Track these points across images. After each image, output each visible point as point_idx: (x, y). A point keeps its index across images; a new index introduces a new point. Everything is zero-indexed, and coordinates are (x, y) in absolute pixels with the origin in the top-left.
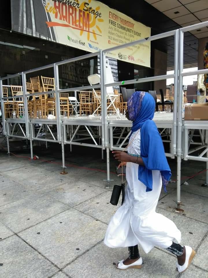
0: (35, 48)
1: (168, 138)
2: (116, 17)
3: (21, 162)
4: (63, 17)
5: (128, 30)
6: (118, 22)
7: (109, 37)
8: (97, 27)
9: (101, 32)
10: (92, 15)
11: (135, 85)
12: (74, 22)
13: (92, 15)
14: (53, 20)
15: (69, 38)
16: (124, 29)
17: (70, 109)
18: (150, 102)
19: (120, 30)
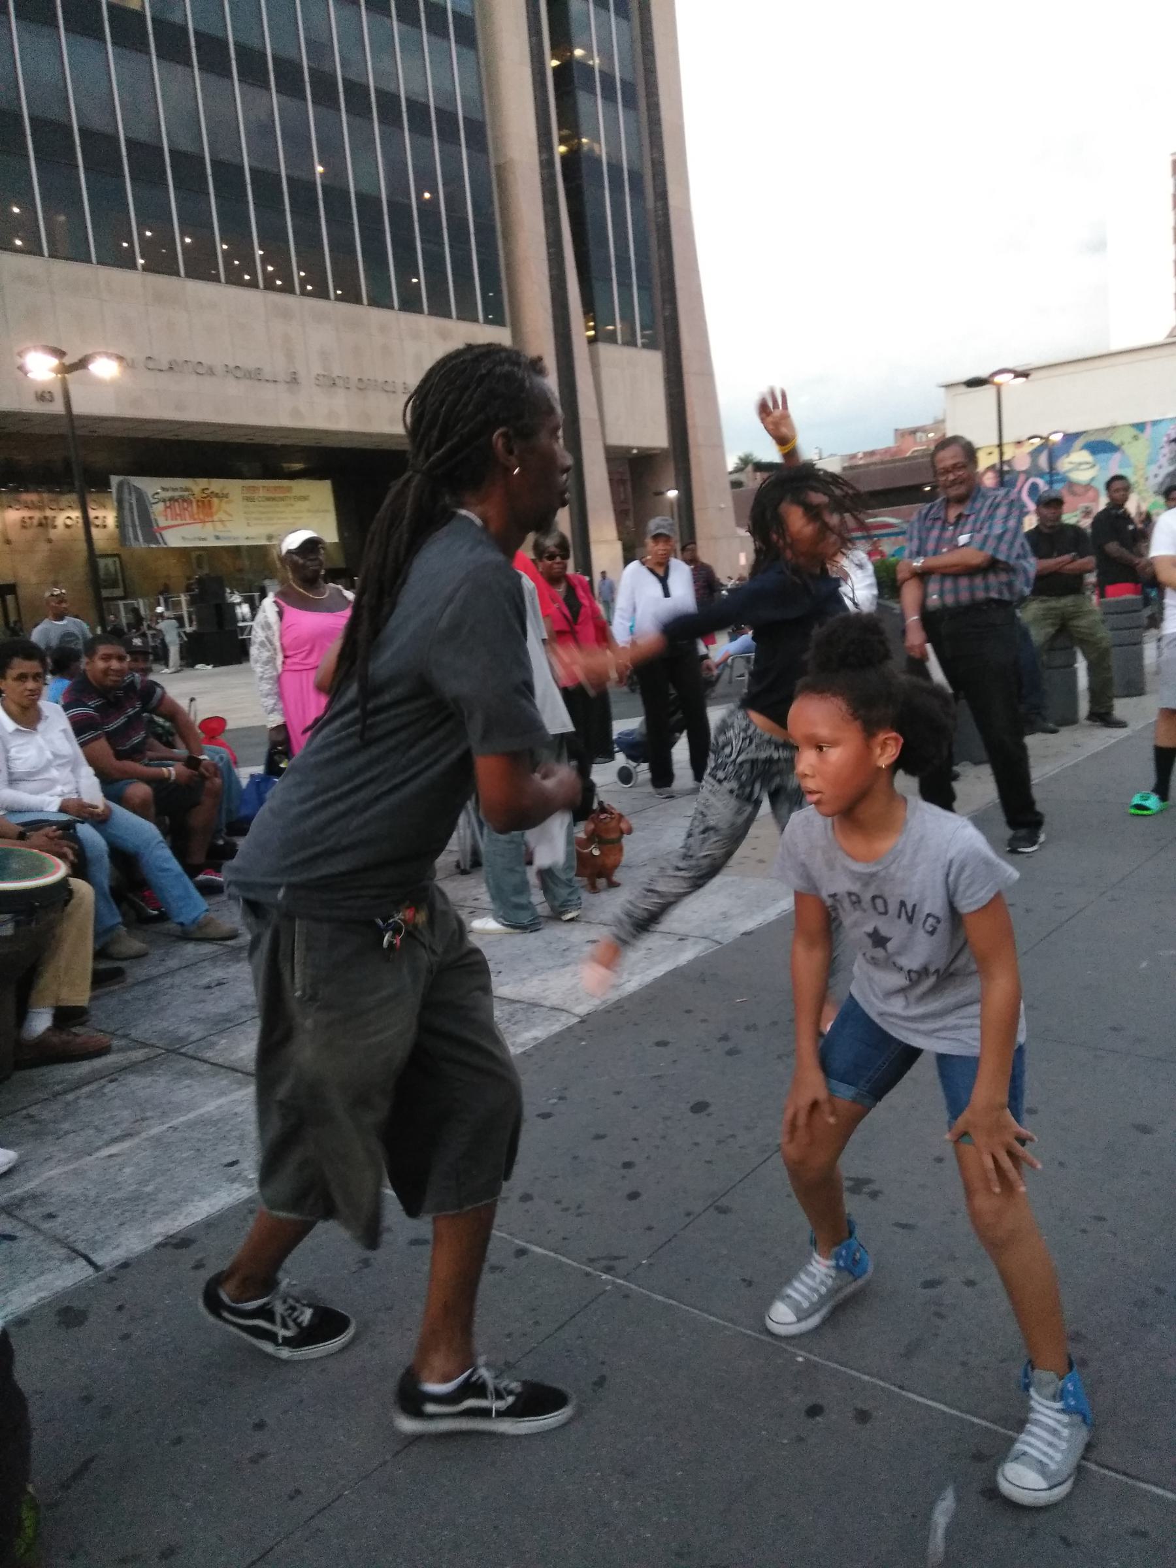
0: (557, 394)
1: (1084, 707)
2: (254, 488)
3: (249, 920)
4: (174, 517)
5: (282, 499)
6: (262, 493)
7: (247, 519)
8: (226, 512)
9: (230, 515)
10: (215, 501)
11: (327, 182)
12: (192, 516)
13: (215, 501)
14: (162, 522)
15: (183, 538)
16: (273, 499)
17: (486, 312)
18: (922, 838)
19: (268, 503)
